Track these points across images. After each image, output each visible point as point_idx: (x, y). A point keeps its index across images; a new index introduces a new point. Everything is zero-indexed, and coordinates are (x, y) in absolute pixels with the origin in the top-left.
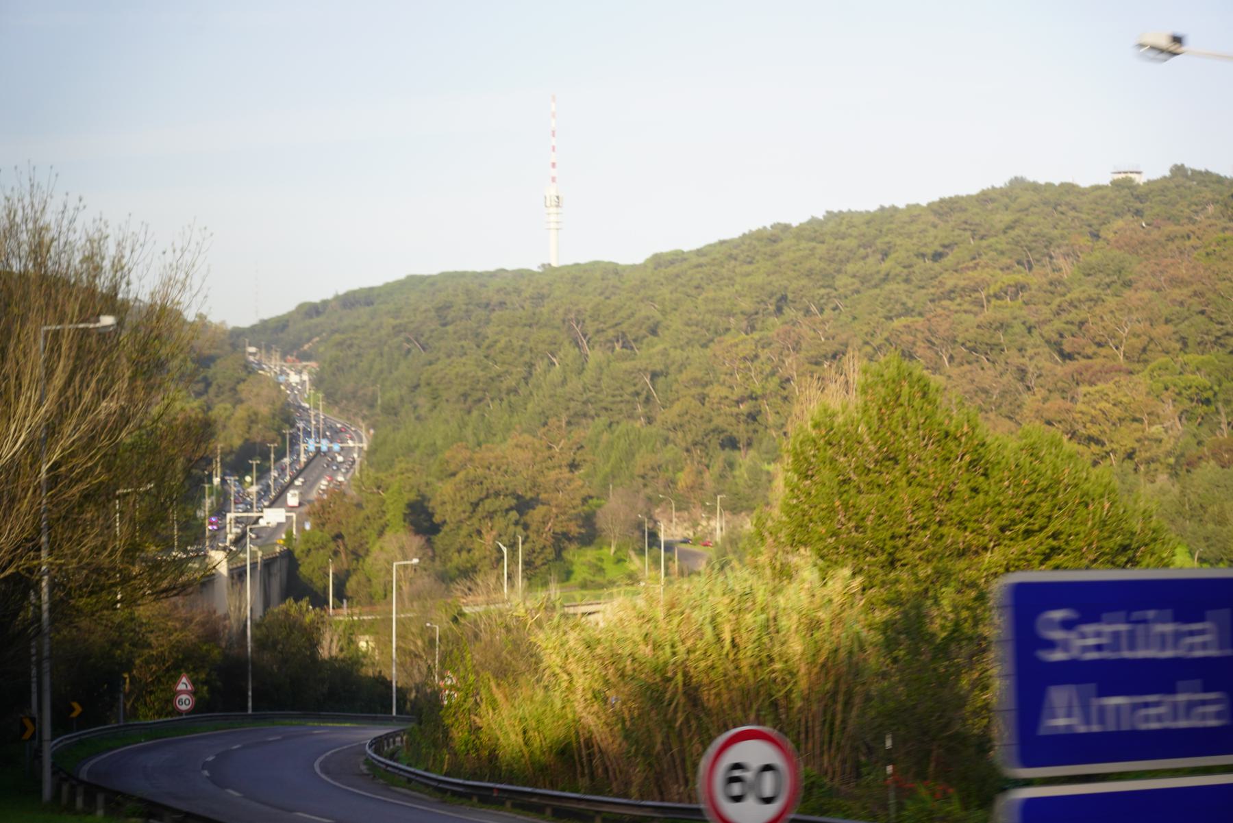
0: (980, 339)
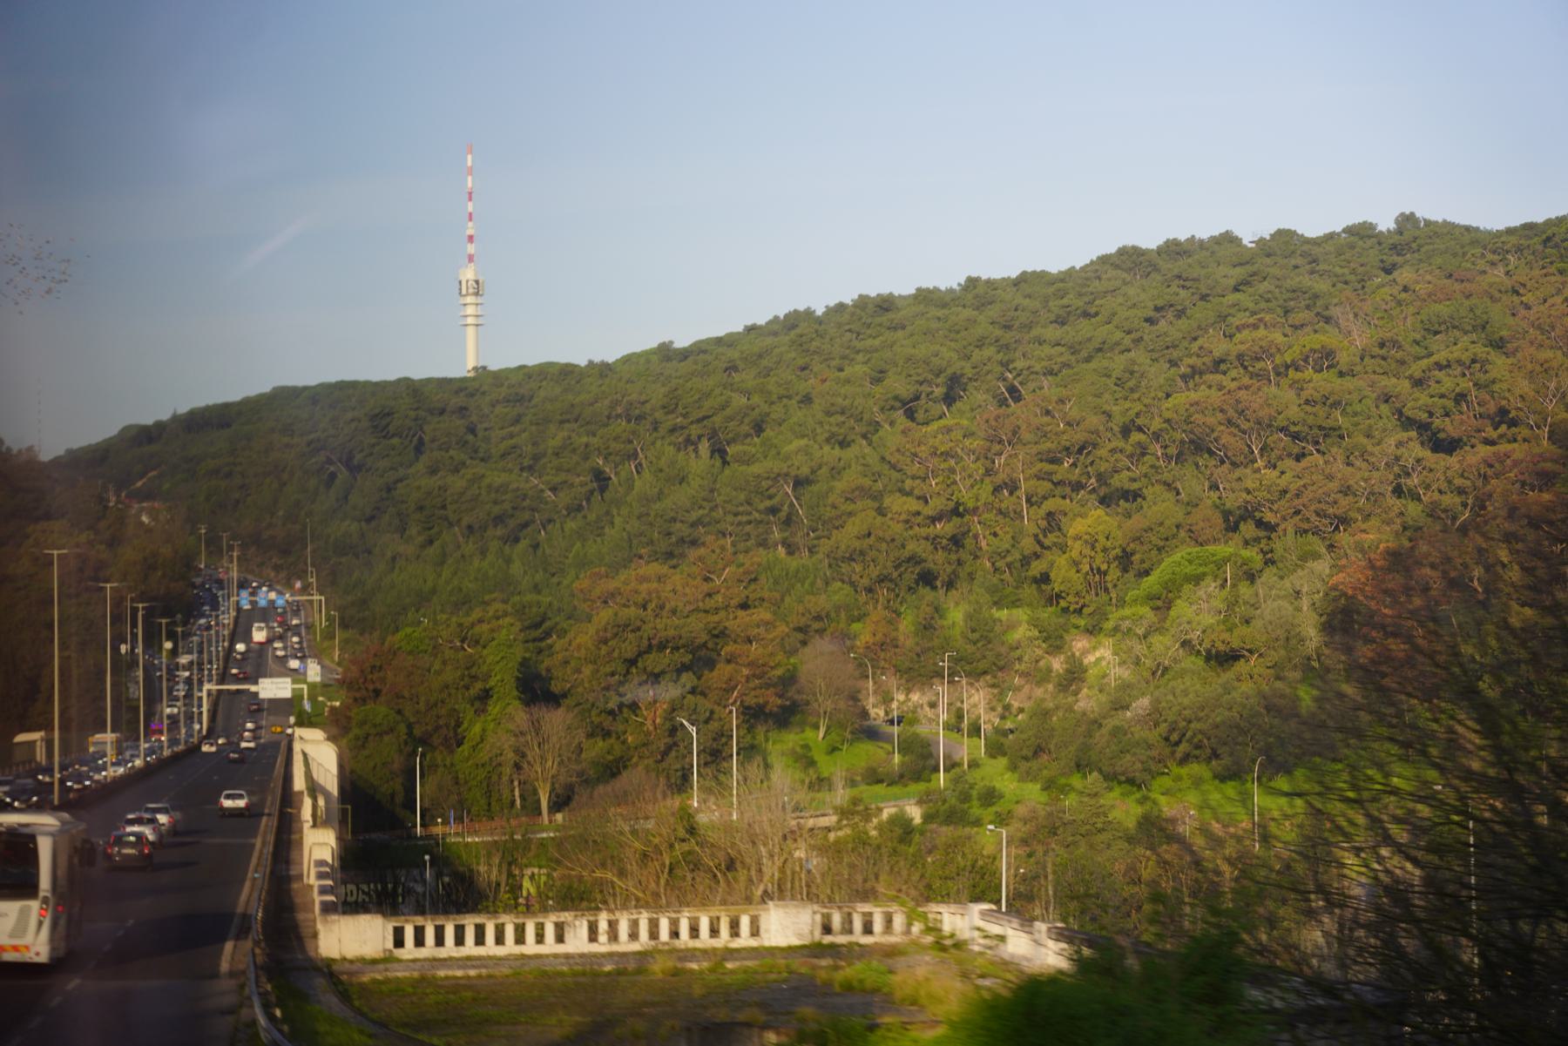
0: (1310, 420)
